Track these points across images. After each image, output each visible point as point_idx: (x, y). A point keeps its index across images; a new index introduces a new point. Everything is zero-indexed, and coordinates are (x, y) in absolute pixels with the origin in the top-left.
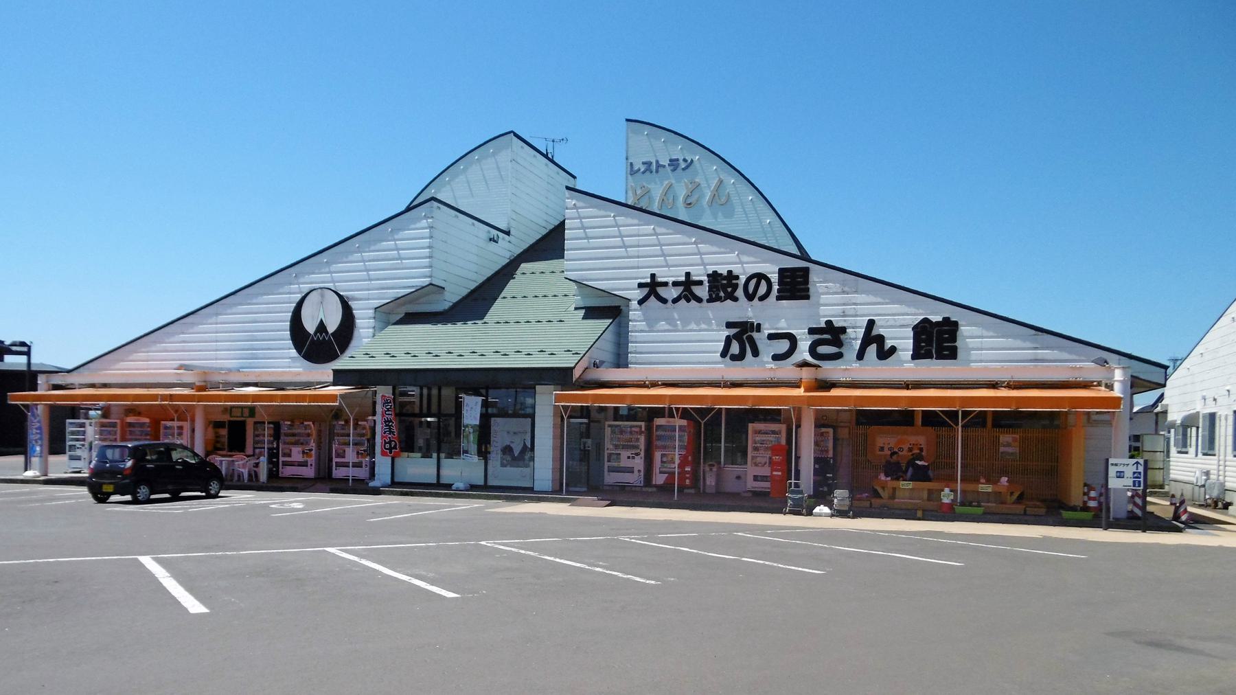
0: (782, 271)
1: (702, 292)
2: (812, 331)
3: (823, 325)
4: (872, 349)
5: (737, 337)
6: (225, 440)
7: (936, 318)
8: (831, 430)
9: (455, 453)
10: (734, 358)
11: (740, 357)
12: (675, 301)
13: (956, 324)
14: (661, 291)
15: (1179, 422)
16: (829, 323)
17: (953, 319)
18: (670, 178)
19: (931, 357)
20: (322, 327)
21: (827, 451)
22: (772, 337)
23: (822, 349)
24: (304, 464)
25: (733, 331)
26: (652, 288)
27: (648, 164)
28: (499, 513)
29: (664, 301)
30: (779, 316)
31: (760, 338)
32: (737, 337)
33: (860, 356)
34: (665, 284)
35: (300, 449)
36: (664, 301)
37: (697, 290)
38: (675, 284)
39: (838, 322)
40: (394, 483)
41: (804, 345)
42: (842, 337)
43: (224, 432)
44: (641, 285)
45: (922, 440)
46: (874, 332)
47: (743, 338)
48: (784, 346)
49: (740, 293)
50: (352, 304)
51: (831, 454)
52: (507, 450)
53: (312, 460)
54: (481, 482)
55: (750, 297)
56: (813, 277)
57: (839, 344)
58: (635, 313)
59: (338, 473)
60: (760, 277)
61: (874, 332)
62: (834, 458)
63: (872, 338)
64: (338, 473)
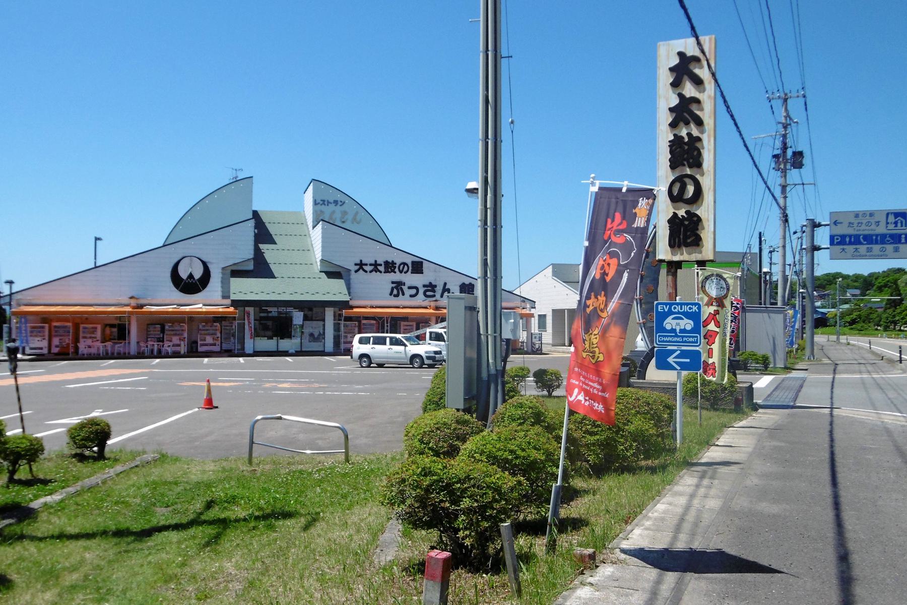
0: (413, 263)
1: (382, 268)
2: (424, 286)
4: (446, 294)
5: (396, 287)
6: (116, 334)
7: (467, 283)
8: (82, 326)
9: (289, 336)
10: (395, 296)
11: (397, 296)
12: (371, 272)
14: (364, 267)
15: (302, 313)
18: (332, 206)
19: (568, 310)
20: (191, 276)
22: (410, 288)
23: (428, 293)
24: (215, 345)
26: (361, 265)
27: (324, 201)
29: (366, 272)
30: (410, 279)
31: (405, 288)
32: (396, 287)
33: (442, 296)
34: (366, 265)
35: (178, 337)
36: (366, 272)
37: (379, 268)
38: (371, 265)
41: (421, 291)
43: (115, 330)
44: (356, 264)
47: (398, 288)
48: (414, 291)
49: (397, 270)
50: (210, 266)
52: (312, 335)
53: (218, 343)
54: (275, 349)
55: (401, 272)
56: (424, 265)
57: (434, 292)
58: (353, 276)
59: (200, 349)
60: (405, 264)
63: (446, 290)
64: (200, 349)
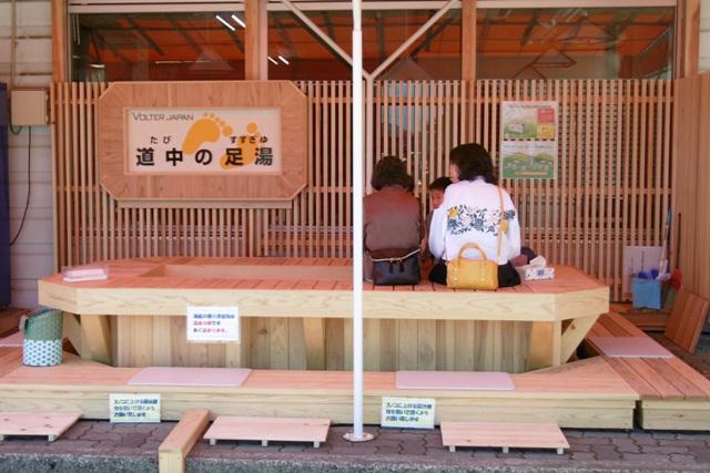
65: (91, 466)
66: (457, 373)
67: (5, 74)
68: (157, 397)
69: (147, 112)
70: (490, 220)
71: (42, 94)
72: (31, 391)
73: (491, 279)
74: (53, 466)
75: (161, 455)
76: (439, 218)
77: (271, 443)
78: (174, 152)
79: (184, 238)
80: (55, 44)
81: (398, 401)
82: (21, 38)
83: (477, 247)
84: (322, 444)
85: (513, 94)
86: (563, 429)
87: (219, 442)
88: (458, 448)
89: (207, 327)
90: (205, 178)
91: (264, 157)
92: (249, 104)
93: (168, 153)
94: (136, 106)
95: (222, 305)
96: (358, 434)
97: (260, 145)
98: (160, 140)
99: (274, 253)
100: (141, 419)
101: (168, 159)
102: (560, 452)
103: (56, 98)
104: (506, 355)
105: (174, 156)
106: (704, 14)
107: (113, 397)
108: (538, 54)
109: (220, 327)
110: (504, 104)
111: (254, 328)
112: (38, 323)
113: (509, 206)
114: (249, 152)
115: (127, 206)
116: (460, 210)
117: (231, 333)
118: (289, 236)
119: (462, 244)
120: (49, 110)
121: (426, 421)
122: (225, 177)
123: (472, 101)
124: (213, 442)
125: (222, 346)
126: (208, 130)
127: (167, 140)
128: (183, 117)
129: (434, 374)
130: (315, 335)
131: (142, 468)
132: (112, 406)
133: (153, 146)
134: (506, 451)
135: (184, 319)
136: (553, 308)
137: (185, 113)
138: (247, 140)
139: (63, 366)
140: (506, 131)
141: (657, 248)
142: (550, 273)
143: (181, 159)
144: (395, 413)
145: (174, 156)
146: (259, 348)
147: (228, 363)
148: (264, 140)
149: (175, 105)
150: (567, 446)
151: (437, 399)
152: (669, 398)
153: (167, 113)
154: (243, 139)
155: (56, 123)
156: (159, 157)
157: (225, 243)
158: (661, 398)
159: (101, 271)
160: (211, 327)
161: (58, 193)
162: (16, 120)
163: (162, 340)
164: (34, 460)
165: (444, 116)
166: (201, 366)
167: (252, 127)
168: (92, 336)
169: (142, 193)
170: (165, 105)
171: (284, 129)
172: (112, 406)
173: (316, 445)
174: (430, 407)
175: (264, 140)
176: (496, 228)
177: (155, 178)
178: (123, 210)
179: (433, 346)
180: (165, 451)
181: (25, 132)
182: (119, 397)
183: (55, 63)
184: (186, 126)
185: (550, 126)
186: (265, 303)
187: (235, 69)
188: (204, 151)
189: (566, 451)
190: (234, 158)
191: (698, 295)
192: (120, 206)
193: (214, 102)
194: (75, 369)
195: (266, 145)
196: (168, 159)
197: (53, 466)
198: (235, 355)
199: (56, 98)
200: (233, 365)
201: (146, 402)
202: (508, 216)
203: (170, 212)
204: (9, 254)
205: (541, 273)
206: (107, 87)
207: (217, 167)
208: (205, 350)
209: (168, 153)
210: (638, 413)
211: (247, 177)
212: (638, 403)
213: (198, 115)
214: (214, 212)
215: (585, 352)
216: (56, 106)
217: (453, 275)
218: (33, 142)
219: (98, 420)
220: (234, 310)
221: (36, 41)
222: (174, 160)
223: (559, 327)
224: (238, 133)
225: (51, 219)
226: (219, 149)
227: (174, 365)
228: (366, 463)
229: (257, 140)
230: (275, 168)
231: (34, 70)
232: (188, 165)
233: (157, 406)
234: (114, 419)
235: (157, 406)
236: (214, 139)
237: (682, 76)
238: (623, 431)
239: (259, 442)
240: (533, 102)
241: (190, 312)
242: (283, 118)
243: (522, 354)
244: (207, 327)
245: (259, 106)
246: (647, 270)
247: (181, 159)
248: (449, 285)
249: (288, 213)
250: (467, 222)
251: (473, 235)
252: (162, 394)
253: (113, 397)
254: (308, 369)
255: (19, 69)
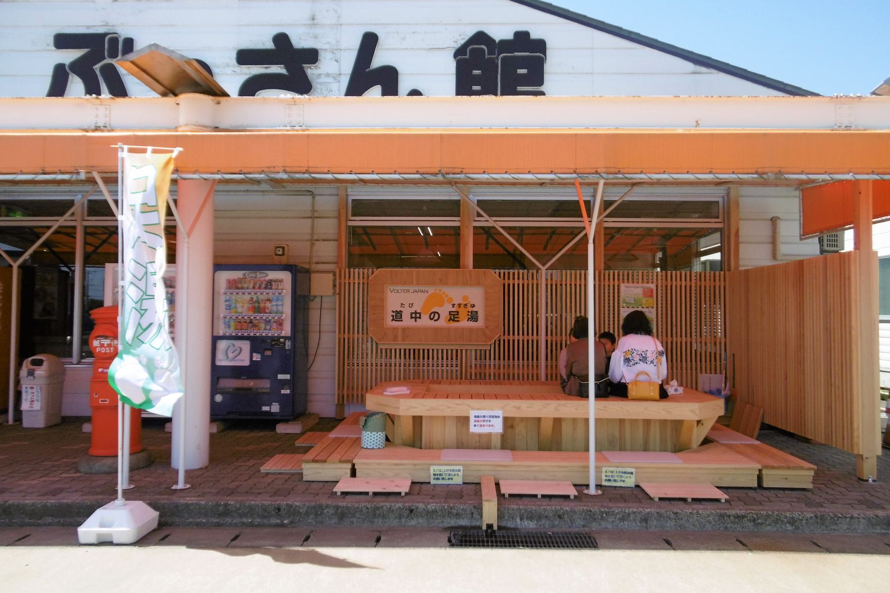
2: (245, 57)
3: (270, 45)
13: (540, 46)
16: (282, 40)
17: (534, 35)
21: (280, 324)
25: (69, 56)
28: (10, 244)
32: (82, 68)
39: (300, 41)
40: (505, 350)
42: (311, 71)
45: (475, 296)
46: (379, 60)
51: (287, 331)
61: (379, 60)
62: (293, 338)
65: (436, 511)
66: (622, 453)
67: (306, 263)
68: (633, 470)
69: (399, 288)
70: (651, 356)
71: (331, 275)
72: (379, 464)
73: (656, 394)
74: (411, 511)
75: (484, 503)
76: (617, 357)
77: (543, 496)
78: (416, 313)
79: (421, 368)
80: (339, 247)
81: (611, 469)
82: (317, 240)
83: (647, 374)
84: (406, 494)
85: (628, 279)
86: (575, 485)
87: (343, 493)
88: (660, 499)
89: (482, 423)
90: (436, 330)
91: (474, 317)
92: (465, 284)
93: (412, 314)
94: (393, 284)
95: (492, 410)
96: (592, 491)
97: (470, 309)
98: (407, 306)
99: (478, 377)
100: (450, 482)
101: (412, 318)
102: (723, 501)
103: (340, 278)
104: (663, 441)
105: (416, 316)
106: (741, 233)
107: (432, 468)
108: (614, 252)
109: (491, 423)
110: (622, 286)
111: (509, 423)
112: (373, 421)
113: (660, 348)
114: (463, 313)
115: (384, 347)
116: (632, 351)
117: (497, 427)
118: (499, 364)
119: (637, 372)
120: (335, 286)
121: (630, 482)
122: (449, 329)
123: (602, 283)
124: (339, 494)
125: (490, 435)
126: (439, 300)
127: (411, 305)
128: (422, 291)
129: (618, 454)
130: (547, 428)
131: (469, 512)
132: (432, 472)
133: (402, 309)
134: (690, 500)
135: (467, 419)
136: (697, 412)
137: (423, 288)
138: (462, 306)
139: (386, 449)
140: (624, 302)
141: (718, 375)
142: (681, 390)
143: (420, 318)
144: (437, 476)
145: (416, 316)
146: (510, 439)
147: (493, 445)
148: (473, 306)
149: (418, 284)
150: (576, 494)
151: (636, 468)
152: (778, 468)
153: (412, 289)
154: (460, 305)
155: (339, 294)
156: (406, 316)
157: (376, 371)
158: (773, 468)
159: (405, 388)
160: (485, 423)
161: (339, 339)
162: (313, 293)
163: (451, 432)
164: (399, 508)
165: (528, 292)
166: (475, 448)
167: (465, 298)
168: (405, 429)
169: (395, 338)
170: (411, 283)
171: (487, 299)
172: (432, 472)
173: (403, 494)
174: (632, 473)
175: (473, 306)
176: (655, 361)
177: (404, 329)
178: (381, 350)
179: (617, 434)
180: (487, 501)
181: (318, 300)
182: (436, 468)
183: (339, 256)
184: (424, 296)
185: (650, 300)
186: (519, 408)
187: (453, 261)
188: (434, 313)
189: (727, 501)
190: (454, 317)
191: (753, 405)
192: (380, 347)
193: (443, 282)
194: (390, 450)
195: (474, 309)
196: (412, 318)
197: (411, 511)
198: (497, 441)
199: (340, 278)
200: (495, 448)
201: (625, 473)
202: (661, 353)
203: (412, 352)
204: (307, 378)
205: (676, 390)
206: (373, 273)
207: (442, 323)
208: (478, 438)
209: (412, 314)
210: (760, 478)
211: (463, 329)
212: (760, 471)
213: (431, 290)
214: (398, 351)
215: (706, 441)
216: (340, 284)
217: (632, 392)
218: (324, 305)
219: (422, 483)
220: (500, 413)
221: (326, 242)
222: (416, 318)
223: (696, 424)
224: (456, 303)
225: (335, 355)
226: (445, 310)
227: (458, 448)
228: (609, 508)
229: (469, 306)
230: (390, 323)
231: (325, 261)
232: (425, 321)
233: (633, 477)
234: (433, 482)
235: (461, 474)
236: (441, 305)
237: (729, 270)
238: (751, 488)
239: (535, 496)
240: (640, 284)
241: (472, 414)
242: (486, 293)
243: (675, 439)
244: (482, 423)
245: (471, 285)
246: (713, 388)
247: (420, 318)
248: (630, 397)
249: (488, 352)
250: (637, 359)
251: (642, 366)
252: (464, 465)
253: (432, 468)
254: (539, 449)
255: (315, 260)
